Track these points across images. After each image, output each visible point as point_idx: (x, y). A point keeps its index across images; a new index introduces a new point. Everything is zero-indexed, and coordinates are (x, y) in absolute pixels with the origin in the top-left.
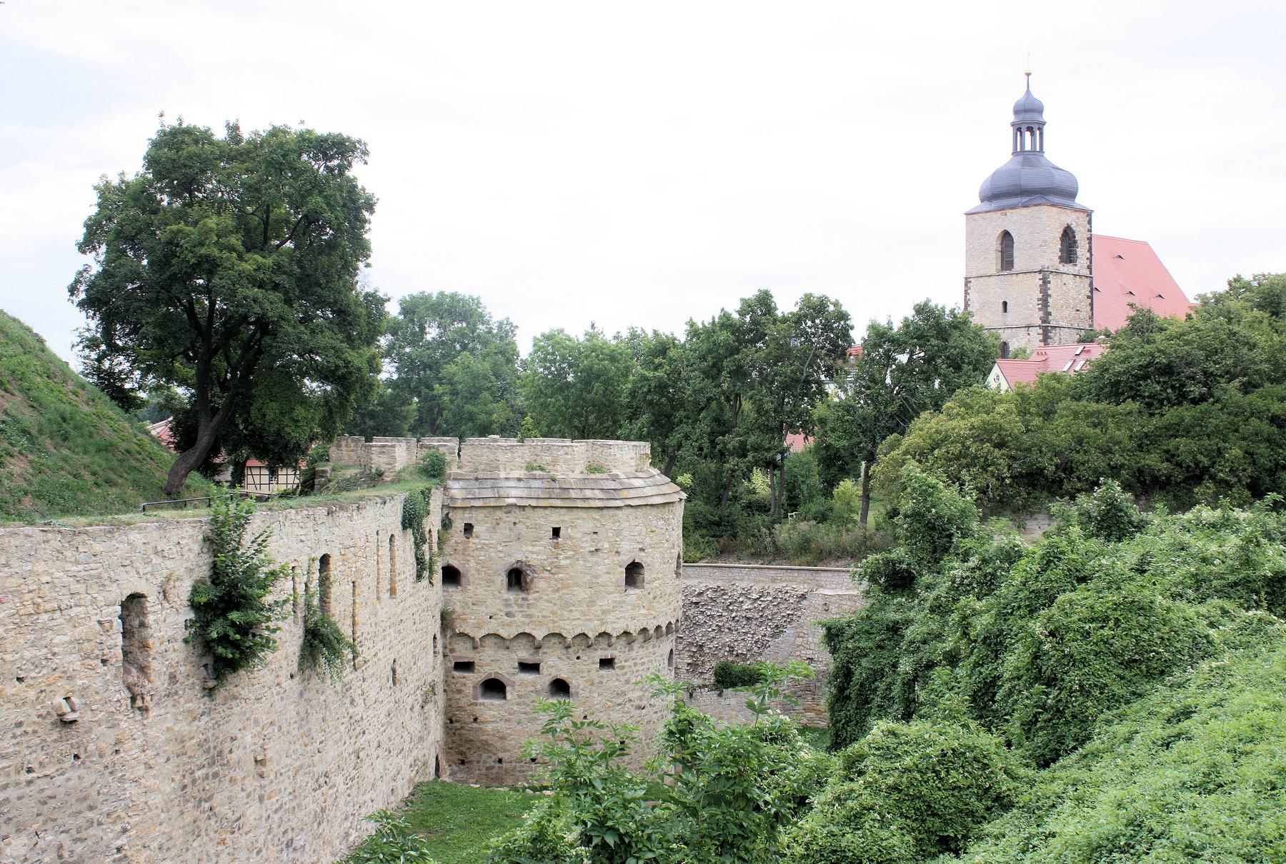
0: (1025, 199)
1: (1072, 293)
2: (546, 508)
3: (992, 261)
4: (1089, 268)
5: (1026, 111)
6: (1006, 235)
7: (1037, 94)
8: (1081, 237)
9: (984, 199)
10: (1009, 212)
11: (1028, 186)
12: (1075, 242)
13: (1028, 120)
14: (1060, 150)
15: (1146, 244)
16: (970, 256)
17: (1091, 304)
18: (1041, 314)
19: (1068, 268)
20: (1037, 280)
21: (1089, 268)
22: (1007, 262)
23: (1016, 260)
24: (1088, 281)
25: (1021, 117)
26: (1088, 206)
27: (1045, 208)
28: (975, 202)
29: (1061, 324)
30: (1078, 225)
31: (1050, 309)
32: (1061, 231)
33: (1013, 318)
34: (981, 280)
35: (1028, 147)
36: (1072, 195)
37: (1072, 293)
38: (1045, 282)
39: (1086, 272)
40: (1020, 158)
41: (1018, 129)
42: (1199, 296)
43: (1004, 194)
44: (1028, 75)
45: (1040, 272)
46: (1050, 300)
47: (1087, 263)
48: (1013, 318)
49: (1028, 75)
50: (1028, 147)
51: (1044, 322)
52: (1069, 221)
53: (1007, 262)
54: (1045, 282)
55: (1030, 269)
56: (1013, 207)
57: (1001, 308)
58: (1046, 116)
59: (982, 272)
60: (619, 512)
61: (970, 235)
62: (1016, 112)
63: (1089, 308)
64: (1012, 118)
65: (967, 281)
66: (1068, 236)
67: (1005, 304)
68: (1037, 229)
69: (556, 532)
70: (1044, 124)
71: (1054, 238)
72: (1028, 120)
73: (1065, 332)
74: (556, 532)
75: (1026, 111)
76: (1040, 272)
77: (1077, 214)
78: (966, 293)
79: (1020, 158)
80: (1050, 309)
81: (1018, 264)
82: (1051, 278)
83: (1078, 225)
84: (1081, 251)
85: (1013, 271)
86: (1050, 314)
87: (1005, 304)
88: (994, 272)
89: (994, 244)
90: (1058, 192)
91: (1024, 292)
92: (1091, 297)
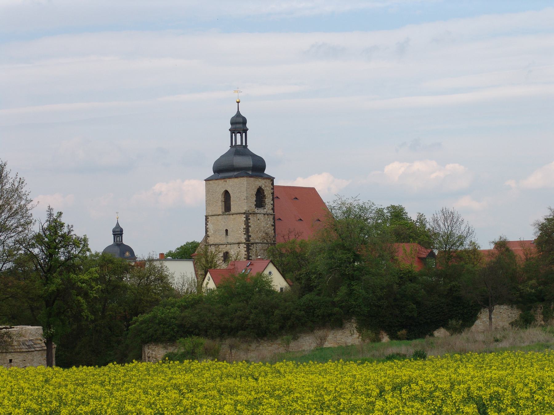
0: (236, 173)
1: (263, 224)
3: (219, 208)
7: (243, 114)
8: (268, 192)
9: (215, 171)
10: (228, 180)
13: (239, 125)
15: (313, 189)
16: (208, 203)
19: (261, 210)
20: (243, 218)
21: (273, 209)
22: (227, 208)
23: (232, 207)
25: (234, 126)
29: (257, 241)
31: (250, 234)
32: (256, 190)
33: (231, 239)
34: (214, 217)
35: (239, 143)
38: (247, 219)
39: (271, 212)
41: (233, 131)
42: (393, 207)
43: (223, 170)
44: (238, 102)
45: (244, 213)
46: (250, 229)
50: (239, 143)
52: (260, 185)
53: (227, 208)
55: (239, 212)
56: (230, 177)
59: (214, 213)
62: (232, 123)
64: (230, 126)
65: (207, 218)
67: (227, 231)
70: (247, 130)
72: (239, 125)
76: (244, 213)
78: (206, 224)
80: (250, 234)
82: (250, 217)
83: (265, 186)
84: (268, 201)
86: (250, 236)
87: (227, 231)
88: (221, 213)
89: (220, 197)
90: (258, 168)
91: (236, 225)
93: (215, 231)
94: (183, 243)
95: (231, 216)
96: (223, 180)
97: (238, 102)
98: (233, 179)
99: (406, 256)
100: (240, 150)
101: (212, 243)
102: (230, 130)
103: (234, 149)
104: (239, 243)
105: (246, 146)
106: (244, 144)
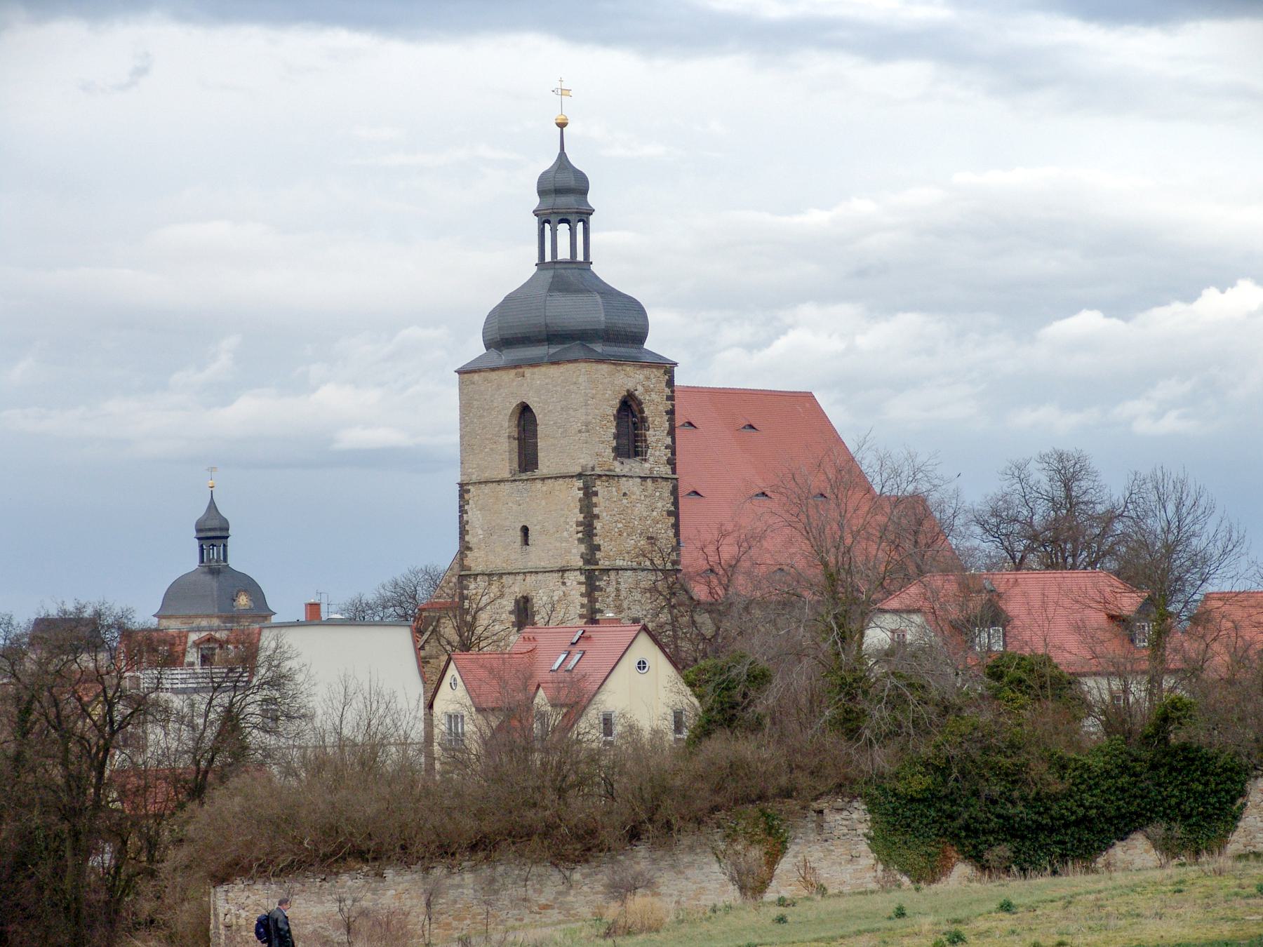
0: (553, 350)
1: (640, 509)
2: (210, 530)
3: (502, 459)
4: (672, 462)
5: (559, 191)
6: (525, 411)
8: (654, 409)
10: (528, 372)
12: (644, 420)
13: (564, 197)
14: (619, 251)
15: (807, 399)
17: (676, 526)
18: (583, 548)
19: (633, 466)
20: (575, 491)
21: (672, 462)
22: (527, 459)
24: (667, 486)
26: (669, 355)
27: (583, 367)
28: (475, 348)
29: (620, 563)
30: (647, 390)
32: (616, 403)
33: (538, 556)
36: (638, 337)
37: (640, 509)
38: (589, 493)
39: (665, 470)
40: (549, 274)
41: (546, 217)
43: (521, 336)
44: (562, 125)
45: (580, 476)
46: (598, 525)
47: (664, 454)
48: (538, 556)
49: (562, 125)
50: (564, 253)
51: (587, 562)
52: (630, 385)
53: (527, 459)
54: (589, 493)
55: (564, 471)
56: (534, 363)
57: (518, 535)
58: (592, 199)
59: (487, 475)
62: (542, 192)
63: (671, 533)
64: (535, 201)
65: (463, 489)
66: (629, 409)
67: (525, 530)
68: (576, 399)
70: (590, 212)
71: (604, 417)
72: (564, 197)
73: (627, 579)
75: (559, 191)
76: (580, 476)
77: (647, 372)
78: (462, 511)
79: (549, 274)
80: (597, 540)
81: (546, 464)
82: (599, 487)
84: (656, 435)
85: (538, 473)
86: (598, 548)
87: (525, 530)
88: (507, 475)
89: (505, 425)
90: (616, 333)
91: (553, 509)
92: (675, 513)
95: (539, 484)
96: (513, 372)
98: (543, 369)
100: (568, 276)
101: (479, 569)
102: (536, 213)
104: (563, 570)
105: (587, 261)
106: (580, 258)
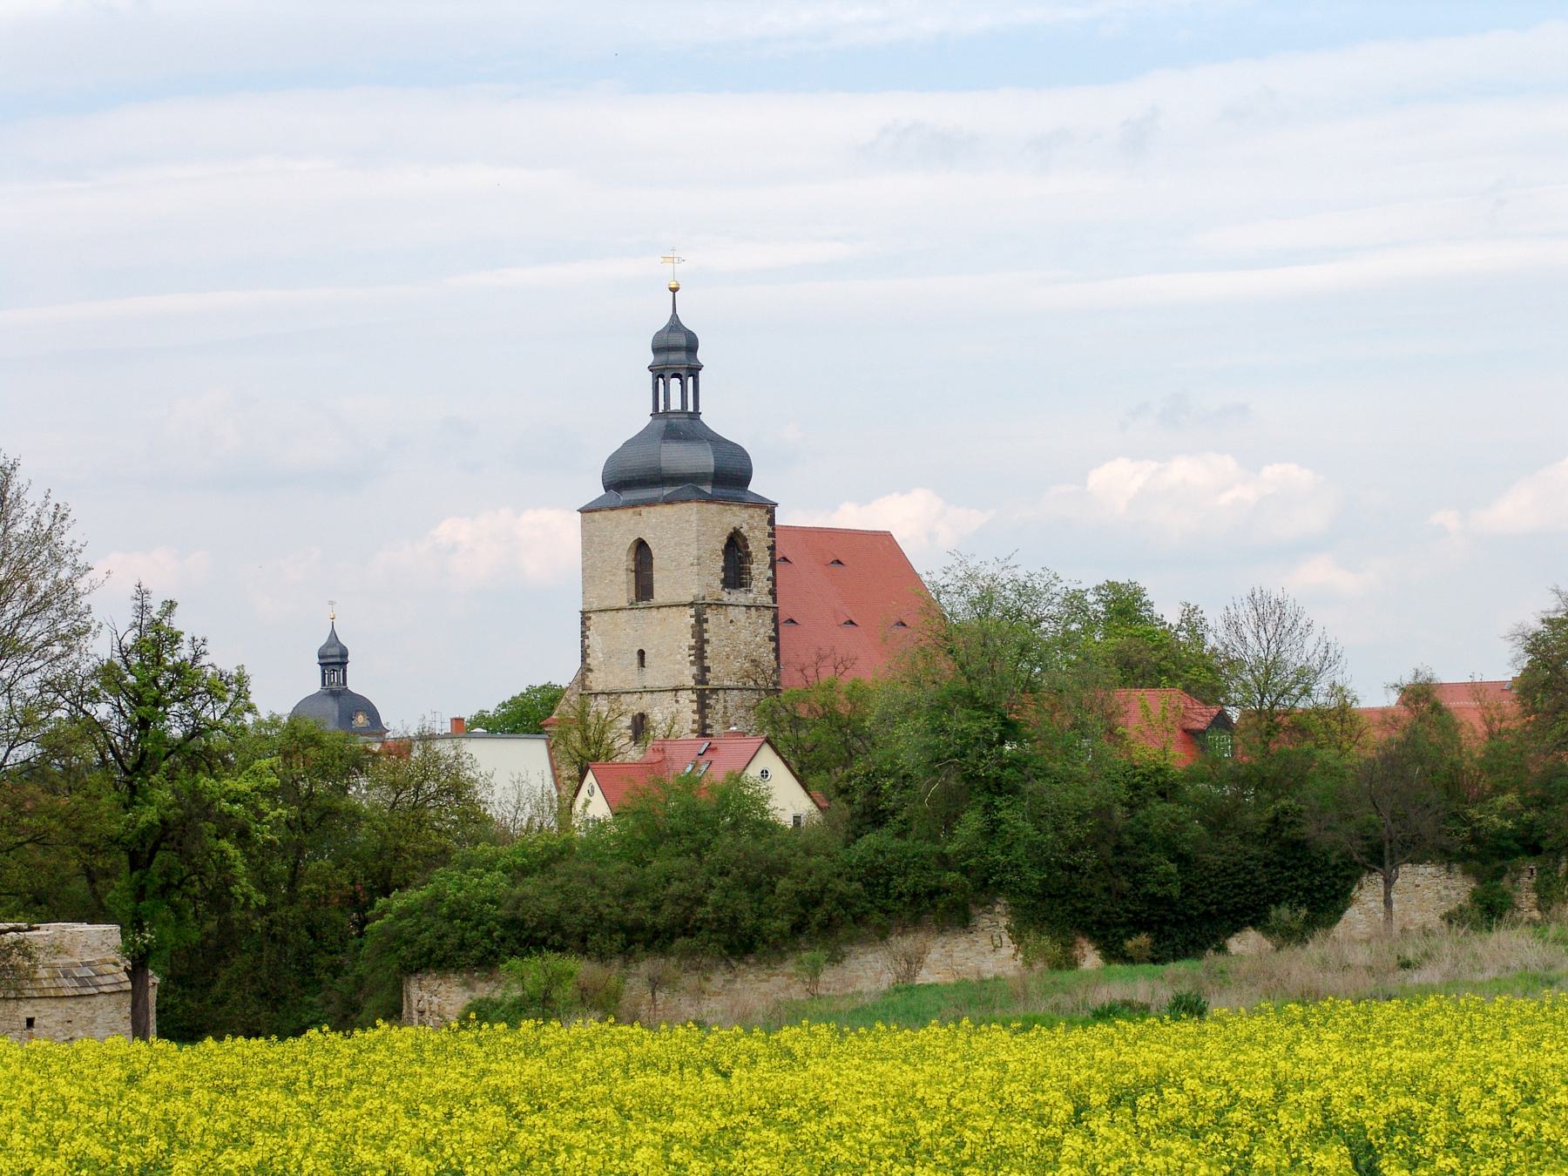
0: (667, 491)
1: (745, 635)
3: (621, 587)
8: (757, 545)
10: (644, 510)
11: (678, 466)
13: (676, 355)
15: (887, 536)
16: (590, 574)
18: (694, 670)
19: (739, 596)
20: (687, 618)
21: (773, 593)
22: (644, 589)
23: (656, 586)
24: (769, 615)
25: (663, 357)
29: (727, 683)
31: (707, 663)
32: (724, 539)
33: (654, 676)
34: (606, 616)
35: (675, 404)
37: (745, 635)
38: (700, 620)
39: (768, 600)
41: (659, 373)
43: (630, 481)
44: (674, 290)
45: (691, 605)
46: (708, 648)
50: (675, 404)
52: (736, 524)
53: (644, 589)
55: (677, 600)
57: (635, 660)
60: (93, 1000)
61: (588, 542)
64: (650, 358)
65: (585, 617)
66: (735, 546)
67: (641, 653)
69: (30, 1022)
70: (699, 368)
72: (676, 355)
74: (30, 1022)
76: (691, 605)
78: (584, 636)
80: (707, 663)
82: (709, 614)
83: (751, 528)
84: (759, 568)
86: (708, 669)
87: (641, 653)
88: (625, 604)
89: (623, 560)
91: (668, 636)
93: (609, 655)
94: (518, 690)
95: (654, 612)
96: (631, 511)
97: (674, 290)
99: (1150, 726)
100: (680, 426)
102: (651, 368)
103: (662, 423)
104: (676, 690)
106: (691, 409)
